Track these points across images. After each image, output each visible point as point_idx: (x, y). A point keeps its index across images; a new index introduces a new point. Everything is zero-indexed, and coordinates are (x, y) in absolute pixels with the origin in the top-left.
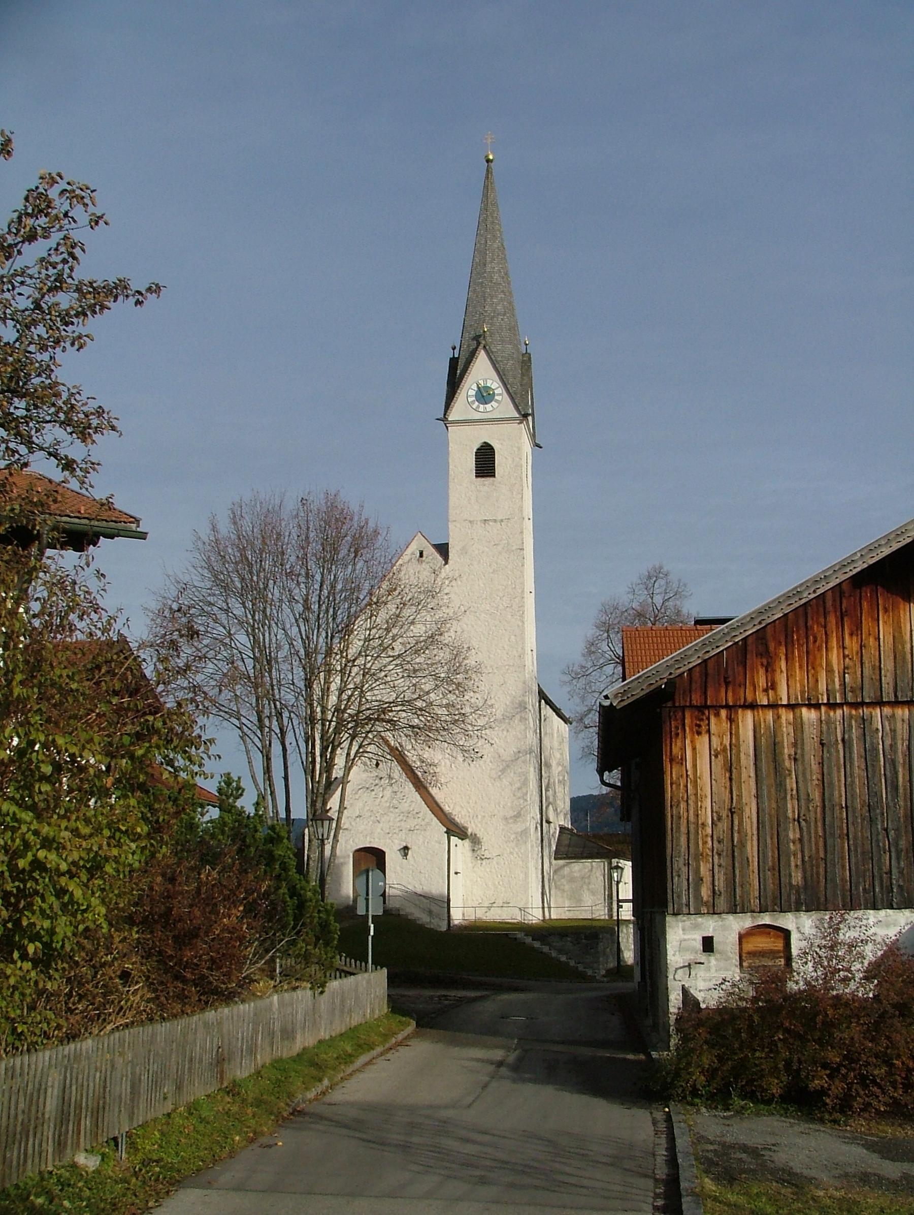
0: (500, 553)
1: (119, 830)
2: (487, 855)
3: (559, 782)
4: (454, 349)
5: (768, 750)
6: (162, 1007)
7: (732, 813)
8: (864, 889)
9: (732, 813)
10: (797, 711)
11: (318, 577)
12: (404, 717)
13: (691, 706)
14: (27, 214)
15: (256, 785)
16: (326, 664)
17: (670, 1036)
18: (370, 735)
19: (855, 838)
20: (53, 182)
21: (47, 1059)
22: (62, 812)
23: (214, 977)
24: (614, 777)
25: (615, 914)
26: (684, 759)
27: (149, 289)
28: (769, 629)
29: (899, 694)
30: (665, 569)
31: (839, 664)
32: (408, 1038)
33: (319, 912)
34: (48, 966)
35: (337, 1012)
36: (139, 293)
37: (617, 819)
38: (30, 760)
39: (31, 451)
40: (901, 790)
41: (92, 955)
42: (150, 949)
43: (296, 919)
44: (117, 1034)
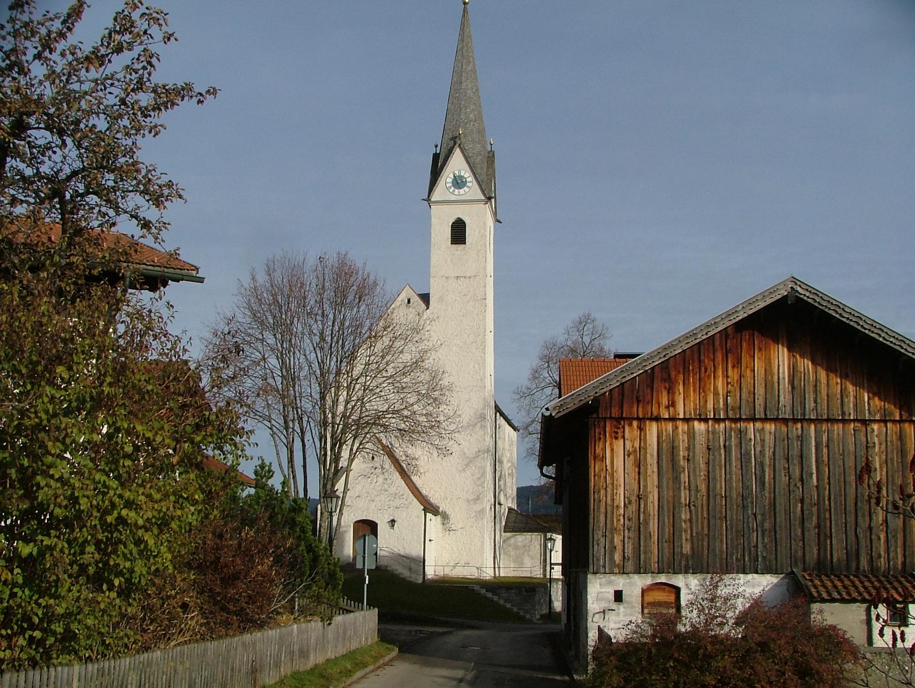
0: (468, 301)
1: (182, 496)
2: (453, 527)
3: (509, 474)
4: (436, 146)
5: (668, 451)
6: (212, 630)
7: (640, 499)
8: (737, 558)
9: (640, 499)
10: (691, 423)
11: (331, 316)
12: (394, 422)
13: (611, 418)
14: (116, 31)
15: (282, 471)
16: (336, 381)
17: (588, 664)
18: (368, 436)
19: (731, 520)
20: (136, 7)
21: (128, 663)
22: (140, 482)
23: (250, 609)
24: (550, 470)
25: (548, 574)
26: (603, 458)
27: (208, 92)
28: (671, 362)
29: (768, 413)
30: (592, 316)
31: (723, 389)
32: (391, 660)
33: (329, 564)
34: (128, 596)
35: (340, 640)
36: (201, 94)
37: (552, 504)
38: (117, 443)
39: (118, 214)
40: (767, 485)
41: (161, 589)
42: (203, 587)
43: (312, 569)
44: (179, 648)
